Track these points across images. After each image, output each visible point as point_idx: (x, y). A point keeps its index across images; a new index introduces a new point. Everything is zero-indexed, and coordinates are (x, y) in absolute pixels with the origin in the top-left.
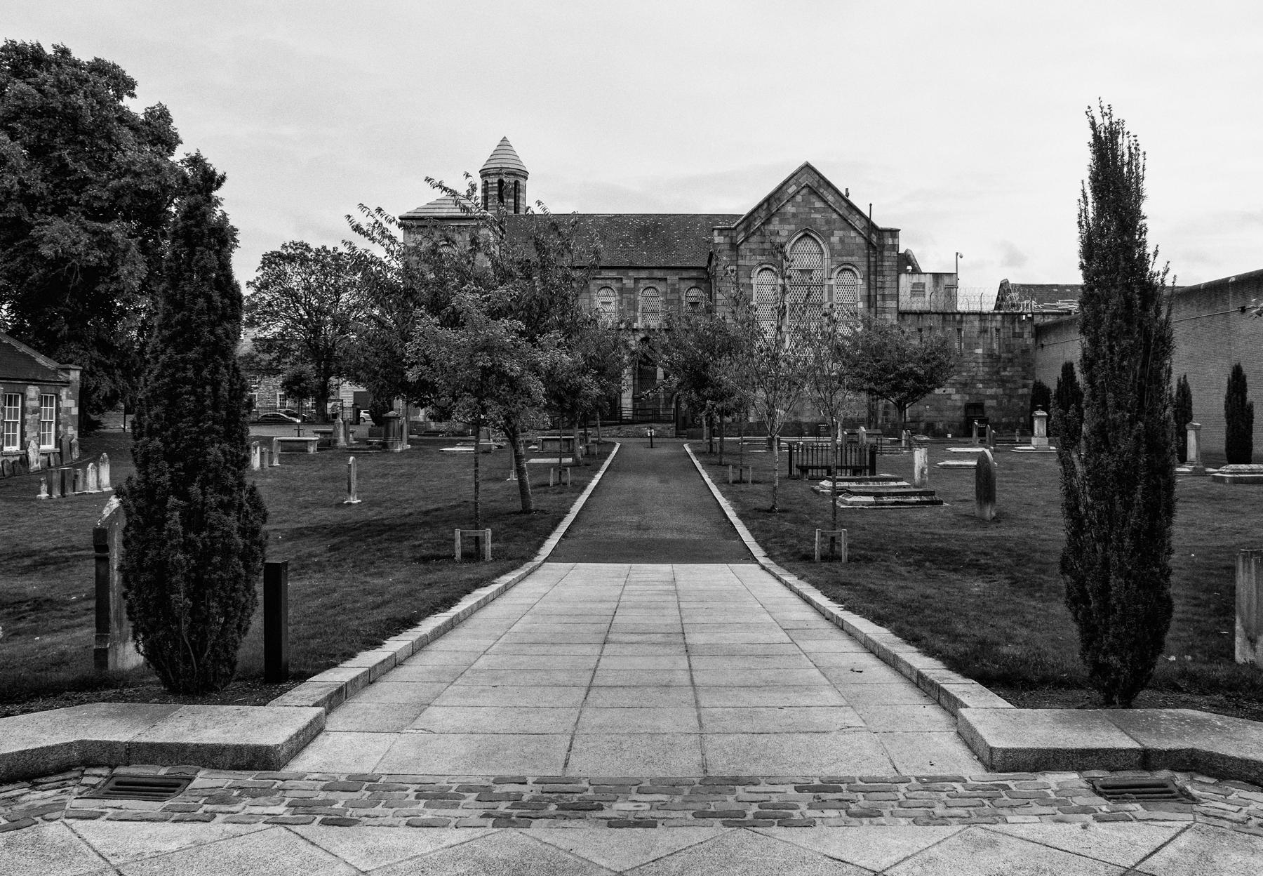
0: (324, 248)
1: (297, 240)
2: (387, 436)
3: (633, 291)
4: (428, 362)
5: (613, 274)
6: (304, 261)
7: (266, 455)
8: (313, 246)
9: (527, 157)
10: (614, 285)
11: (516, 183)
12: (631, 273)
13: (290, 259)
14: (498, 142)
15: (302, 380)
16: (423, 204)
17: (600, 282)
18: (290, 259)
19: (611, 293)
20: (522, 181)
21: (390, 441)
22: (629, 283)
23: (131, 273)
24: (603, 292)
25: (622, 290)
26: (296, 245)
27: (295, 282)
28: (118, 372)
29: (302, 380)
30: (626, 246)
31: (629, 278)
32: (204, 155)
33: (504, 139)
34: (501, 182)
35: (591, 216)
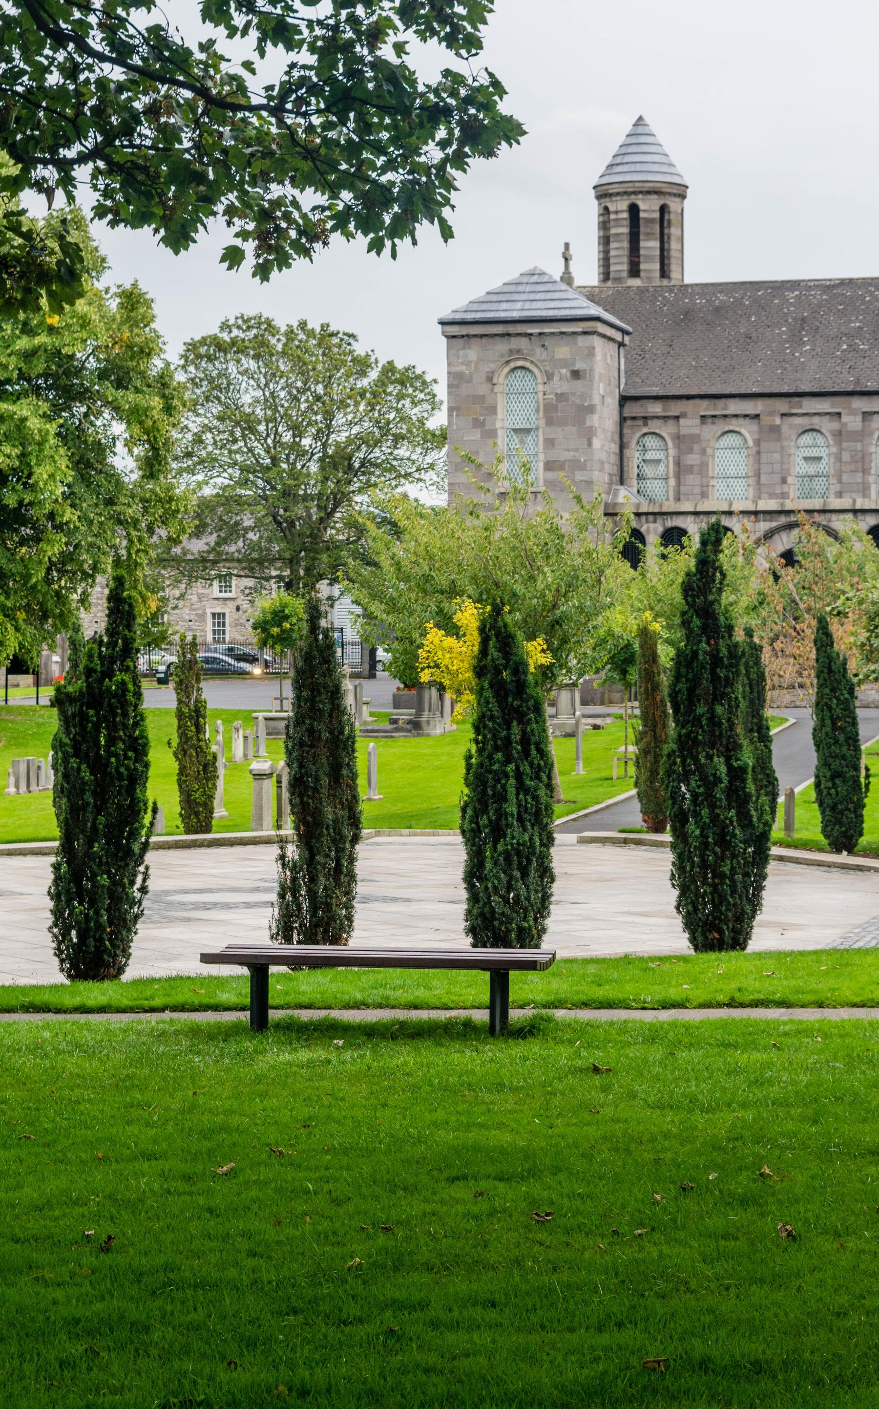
0: (303, 325)
1: (250, 312)
2: (420, 710)
3: (861, 435)
4: (437, 666)
5: (824, 405)
6: (260, 349)
7: (250, 740)
8: (281, 324)
9: (683, 154)
10: (826, 425)
11: (663, 209)
12: (859, 404)
13: (237, 348)
14: (628, 128)
15: (286, 618)
16: (479, 293)
17: (798, 421)
18: (237, 348)
19: (820, 440)
20: (673, 204)
21: (424, 719)
22: (853, 422)
23: (52, 476)
24: (807, 439)
25: (839, 435)
26: (246, 323)
27: (248, 396)
28: (21, 616)
29: (286, 618)
30: (852, 348)
31: (853, 412)
32: (143, 287)
33: (640, 118)
34: (634, 210)
35: (794, 284)
